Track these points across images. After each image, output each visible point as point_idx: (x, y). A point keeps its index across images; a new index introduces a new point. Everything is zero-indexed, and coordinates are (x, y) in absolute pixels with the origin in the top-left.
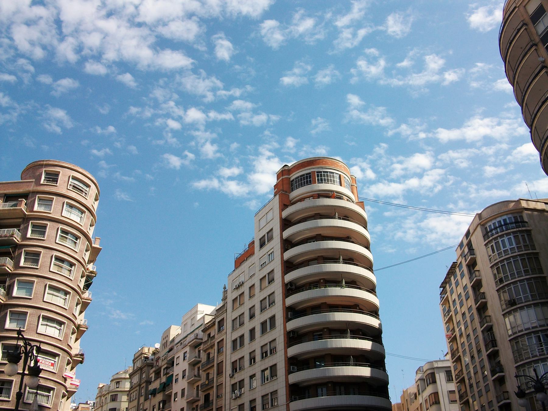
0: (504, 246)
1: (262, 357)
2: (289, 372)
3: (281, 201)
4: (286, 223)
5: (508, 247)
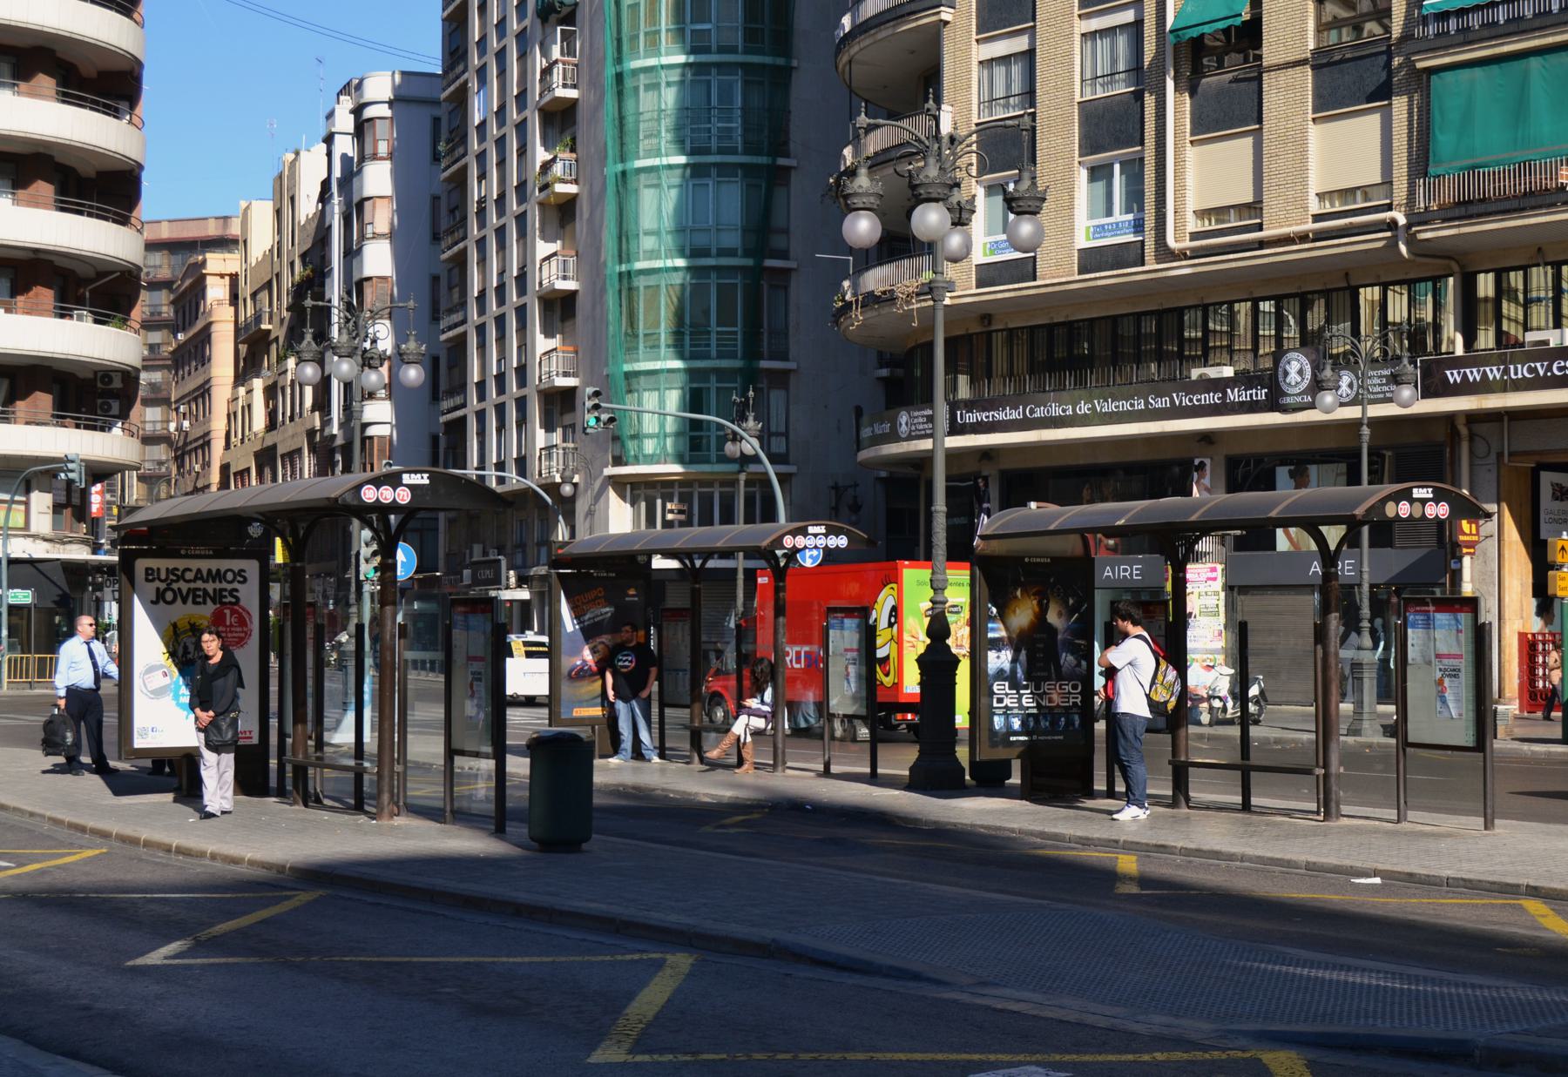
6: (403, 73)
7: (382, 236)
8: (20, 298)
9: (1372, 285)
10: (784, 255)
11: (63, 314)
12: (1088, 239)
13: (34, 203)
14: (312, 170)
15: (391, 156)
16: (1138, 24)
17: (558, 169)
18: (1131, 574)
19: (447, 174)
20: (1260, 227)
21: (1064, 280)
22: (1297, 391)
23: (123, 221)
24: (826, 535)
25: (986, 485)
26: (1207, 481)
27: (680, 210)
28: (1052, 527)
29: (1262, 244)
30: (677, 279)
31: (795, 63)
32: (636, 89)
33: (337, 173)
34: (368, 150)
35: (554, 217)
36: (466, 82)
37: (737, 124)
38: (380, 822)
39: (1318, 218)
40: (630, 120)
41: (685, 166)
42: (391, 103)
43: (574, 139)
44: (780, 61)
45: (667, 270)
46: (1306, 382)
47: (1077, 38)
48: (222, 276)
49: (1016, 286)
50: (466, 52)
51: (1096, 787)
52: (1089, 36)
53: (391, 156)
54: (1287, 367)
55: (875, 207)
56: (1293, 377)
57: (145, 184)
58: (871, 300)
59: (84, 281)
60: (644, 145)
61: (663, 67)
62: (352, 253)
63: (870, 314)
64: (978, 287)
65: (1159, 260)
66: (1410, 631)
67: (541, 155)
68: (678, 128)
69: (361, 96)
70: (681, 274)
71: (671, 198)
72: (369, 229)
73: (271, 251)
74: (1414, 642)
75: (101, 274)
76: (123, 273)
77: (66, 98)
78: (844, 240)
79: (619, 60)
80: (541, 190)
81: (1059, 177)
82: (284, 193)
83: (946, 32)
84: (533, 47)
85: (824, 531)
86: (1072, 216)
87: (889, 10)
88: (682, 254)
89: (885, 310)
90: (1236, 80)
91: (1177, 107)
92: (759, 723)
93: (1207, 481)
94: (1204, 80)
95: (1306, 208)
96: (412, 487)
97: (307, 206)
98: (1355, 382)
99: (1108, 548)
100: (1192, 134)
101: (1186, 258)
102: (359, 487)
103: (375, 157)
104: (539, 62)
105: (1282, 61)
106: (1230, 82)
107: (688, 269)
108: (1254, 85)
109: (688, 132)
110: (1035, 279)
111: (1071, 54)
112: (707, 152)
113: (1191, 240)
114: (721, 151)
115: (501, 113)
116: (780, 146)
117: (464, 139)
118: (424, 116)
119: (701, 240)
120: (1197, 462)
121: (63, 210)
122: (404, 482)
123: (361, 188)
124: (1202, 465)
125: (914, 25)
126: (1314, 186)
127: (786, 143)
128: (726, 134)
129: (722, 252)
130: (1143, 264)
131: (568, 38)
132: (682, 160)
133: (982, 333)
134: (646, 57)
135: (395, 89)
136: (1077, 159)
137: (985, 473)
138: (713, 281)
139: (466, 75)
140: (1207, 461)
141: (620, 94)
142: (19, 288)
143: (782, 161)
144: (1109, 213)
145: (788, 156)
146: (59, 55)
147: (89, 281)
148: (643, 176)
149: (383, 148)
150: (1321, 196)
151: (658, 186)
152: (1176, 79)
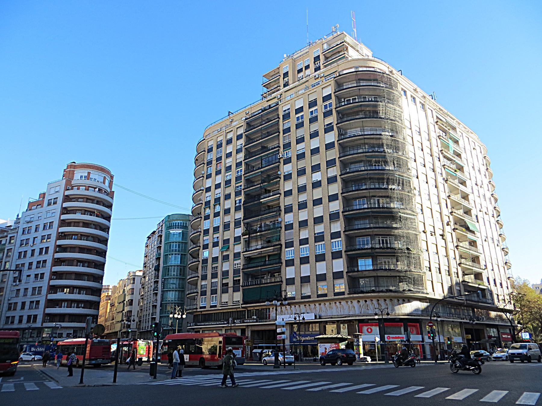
0: (173, 247)
1: (44, 229)
2: (51, 279)
3: (66, 185)
4: (67, 198)
5: (174, 249)
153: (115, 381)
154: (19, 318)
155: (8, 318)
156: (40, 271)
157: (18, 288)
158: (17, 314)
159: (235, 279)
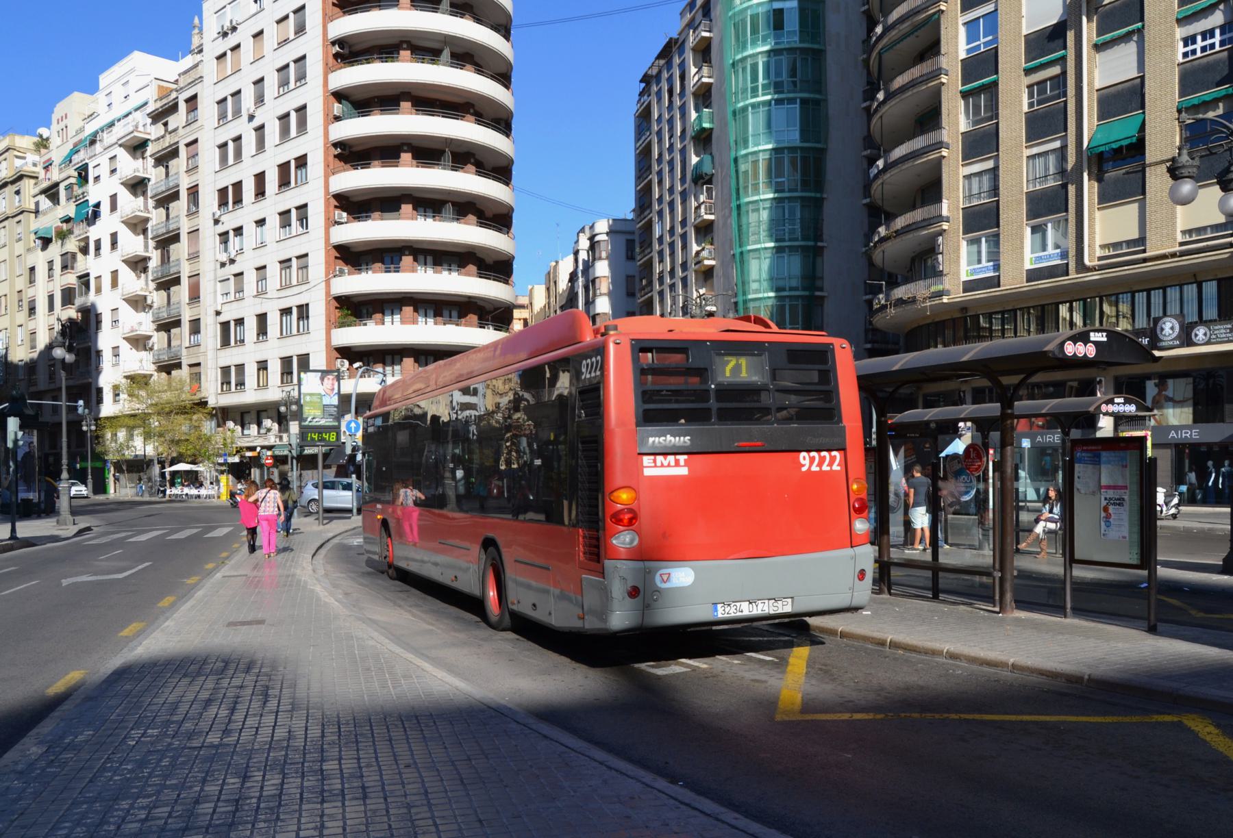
6: (614, 220)
7: (605, 294)
8: (463, 320)
9: (1126, 293)
10: (821, 289)
11: (445, 324)
12: (1031, 264)
13: (468, 274)
14: (566, 267)
15: (607, 258)
16: (1064, 148)
17: (705, 254)
18: (1054, 440)
19: (641, 262)
20: (1144, 251)
21: (1018, 286)
22: (1170, 338)
23: (506, 282)
24: (1124, 404)
25: (964, 396)
26: (1103, 389)
27: (771, 268)
28: (1043, 412)
29: (1145, 260)
30: (770, 303)
31: (825, 196)
32: (748, 212)
33: (581, 267)
34: (597, 255)
35: (701, 277)
36: (651, 218)
37: (798, 226)
38: (1005, 615)
39: (1181, 244)
40: (744, 227)
41: (774, 247)
42: (607, 234)
43: (712, 239)
44: (818, 195)
45: (765, 298)
46: (1176, 334)
47: (1025, 158)
48: (520, 319)
49: (988, 291)
50: (651, 203)
51: (1158, 558)
52: (968, 177)
53: (607, 258)
54: (1163, 326)
55: (1195, 175)
56: (1167, 330)
57: (515, 266)
58: (900, 302)
59: (489, 312)
60: (752, 238)
61: (761, 200)
62: (589, 303)
63: (898, 310)
64: (964, 292)
65: (1078, 272)
66: (1076, 465)
67: (695, 248)
68: (770, 229)
69: (594, 231)
70: (772, 300)
71: (766, 264)
72: (598, 292)
73: (545, 307)
74: (1080, 475)
75: (496, 309)
76: (505, 308)
77: (481, 225)
78: (846, 339)
79: (738, 198)
80: (695, 264)
81: (1014, 232)
82: (551, 280)
83: (944, 162)
84: (690, 197)
85: (1123, 401)
86: (1022, 253)
87: (910, 153)
88: (772, 290)
89: (909, 307)
90: (1127, 173)
91: (1090, 188)
92: (1052, 526)
93: (1103, 389)
94: (1106, 175)
95: (1175, 239)
96: (1096, 343)
97: (563, 284)
98: (1208, 333)
99: (1038, 426)
100: (1099, 204)
101: (1096, 270)
102: (1062, 344)
103: (600, 258)
104: (694, 204)
105: (1159, 160)
106: (1124, 174)
107: (776, 297)
108: (1140, 175)
109: (774, 231)
110: (999, 286)
111: (1021, 167)
112: (784, 240)
113: (1098, 261)
114: (790, 240)
115: (672, 231)
116: (818, 237)
117: (650, 245)
118: (622, 239)
119: (781, 283)
120: (1098, 379)
121: (480, 277)
122: (1092, 339)
123: (594, 273)
124: (1101, 381)
125: (926, 159)
126: (1180, 228)
127: (821, 235)
128: (792, 231)
129: (791, 289)
130: (1068, 275)
131: (709, 191)
132: (772, 244)
133: (960, 318)
134: (752, 196)
135: (610, 227)
136: (1025, 222)
137: (963, 389)
138: (787, 303)
139: (651, 215)
140: (1103, 379)
141: (739, 215)
142: (462, 315)
143: (820, 244)
144: (979, 262)
145: (822, 241)
146: (477, 206)
147: (490, 312)
148: (751, 254)
149: (604, 255)
150: (1184, 232)
151: (759, 258)
152: (1089, 175)
153: (1125, 487)
154: (912, 592)
155: (226, 370)
156: (291, 199)
157: (235, 269)
158: (248, 354)
159: (1139, 25)
